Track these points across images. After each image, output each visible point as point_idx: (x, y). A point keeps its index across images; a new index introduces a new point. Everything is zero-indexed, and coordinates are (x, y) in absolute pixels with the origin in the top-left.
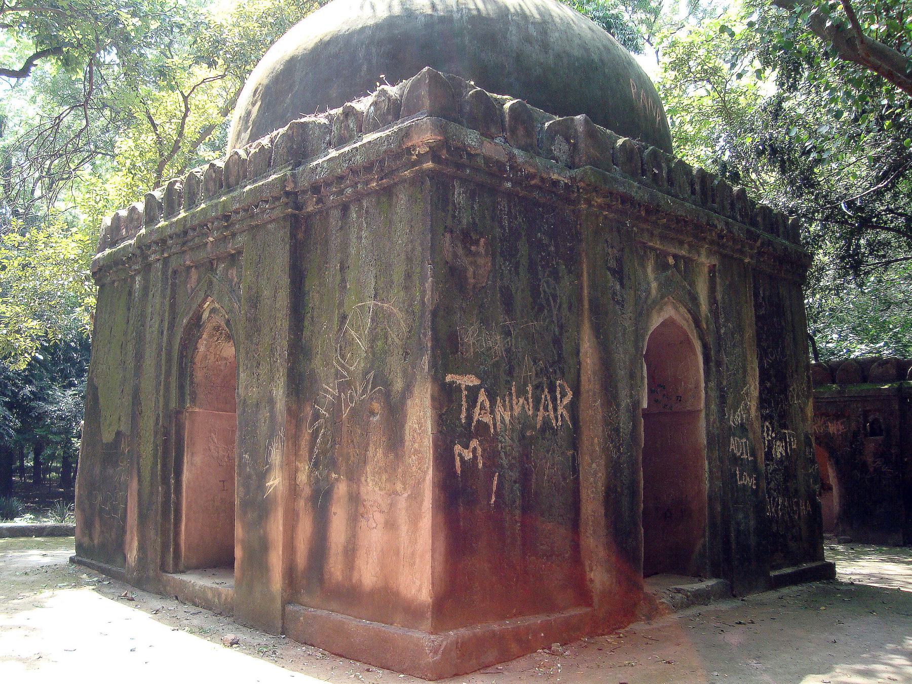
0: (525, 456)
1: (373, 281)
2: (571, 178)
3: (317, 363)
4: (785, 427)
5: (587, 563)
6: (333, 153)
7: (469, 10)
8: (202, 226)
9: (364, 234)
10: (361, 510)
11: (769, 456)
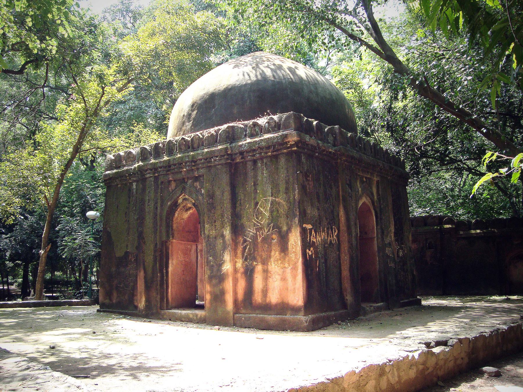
0: (326, 254)
1: (270, 190)
2: (335, 150)
3: (244, 220)
4: (402, 244)
5: (345, 293)
6: (249, 140)
7: (288, 78)
8: (180, 164)
9: (265, 172)
10: (269, 275)
11: (398, 256)
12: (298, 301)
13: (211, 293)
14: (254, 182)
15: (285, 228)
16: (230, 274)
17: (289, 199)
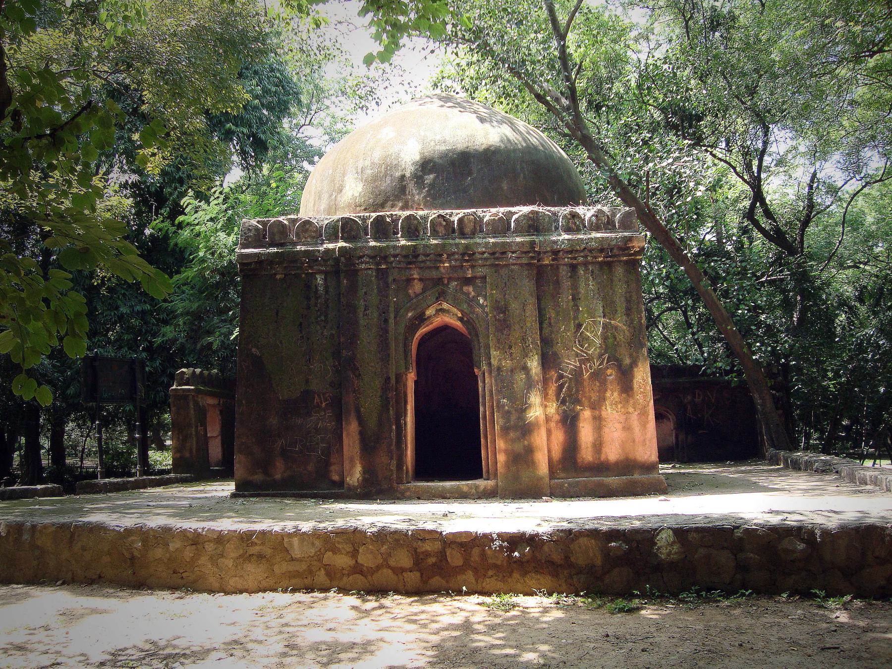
3: (559, 348)
10: (604, 423)
12: (650, 456)
13: (506, 451)
15: (627, 361)
17: (632, 323)
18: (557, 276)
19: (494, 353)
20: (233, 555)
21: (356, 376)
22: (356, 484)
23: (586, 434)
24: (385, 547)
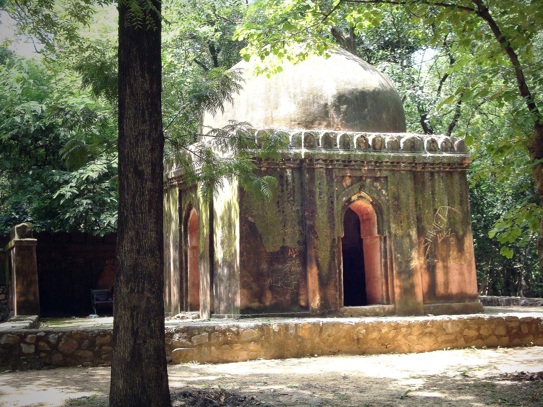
3: (425, 223)
13: (400, 287)
14: (432, 191)
15: (461, 233)
16: (418, 269)
17: (463, 210)
18: (424, 178)
19: (393, 226)
20: (416, 334)
21: (316, 238)
22: (317, 308)
23: (440, 277)
24: (493, 325)
